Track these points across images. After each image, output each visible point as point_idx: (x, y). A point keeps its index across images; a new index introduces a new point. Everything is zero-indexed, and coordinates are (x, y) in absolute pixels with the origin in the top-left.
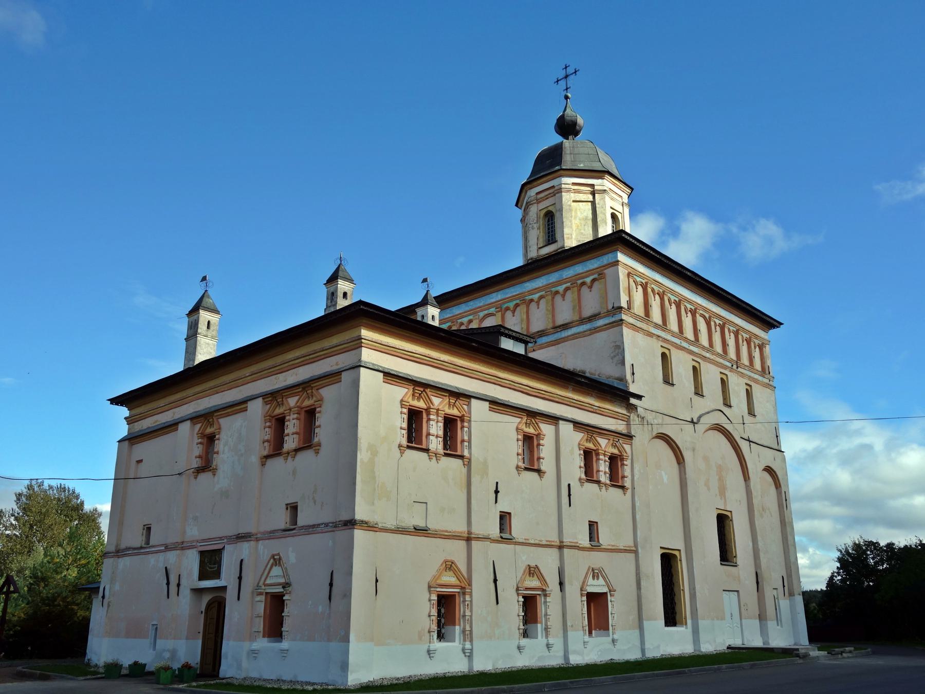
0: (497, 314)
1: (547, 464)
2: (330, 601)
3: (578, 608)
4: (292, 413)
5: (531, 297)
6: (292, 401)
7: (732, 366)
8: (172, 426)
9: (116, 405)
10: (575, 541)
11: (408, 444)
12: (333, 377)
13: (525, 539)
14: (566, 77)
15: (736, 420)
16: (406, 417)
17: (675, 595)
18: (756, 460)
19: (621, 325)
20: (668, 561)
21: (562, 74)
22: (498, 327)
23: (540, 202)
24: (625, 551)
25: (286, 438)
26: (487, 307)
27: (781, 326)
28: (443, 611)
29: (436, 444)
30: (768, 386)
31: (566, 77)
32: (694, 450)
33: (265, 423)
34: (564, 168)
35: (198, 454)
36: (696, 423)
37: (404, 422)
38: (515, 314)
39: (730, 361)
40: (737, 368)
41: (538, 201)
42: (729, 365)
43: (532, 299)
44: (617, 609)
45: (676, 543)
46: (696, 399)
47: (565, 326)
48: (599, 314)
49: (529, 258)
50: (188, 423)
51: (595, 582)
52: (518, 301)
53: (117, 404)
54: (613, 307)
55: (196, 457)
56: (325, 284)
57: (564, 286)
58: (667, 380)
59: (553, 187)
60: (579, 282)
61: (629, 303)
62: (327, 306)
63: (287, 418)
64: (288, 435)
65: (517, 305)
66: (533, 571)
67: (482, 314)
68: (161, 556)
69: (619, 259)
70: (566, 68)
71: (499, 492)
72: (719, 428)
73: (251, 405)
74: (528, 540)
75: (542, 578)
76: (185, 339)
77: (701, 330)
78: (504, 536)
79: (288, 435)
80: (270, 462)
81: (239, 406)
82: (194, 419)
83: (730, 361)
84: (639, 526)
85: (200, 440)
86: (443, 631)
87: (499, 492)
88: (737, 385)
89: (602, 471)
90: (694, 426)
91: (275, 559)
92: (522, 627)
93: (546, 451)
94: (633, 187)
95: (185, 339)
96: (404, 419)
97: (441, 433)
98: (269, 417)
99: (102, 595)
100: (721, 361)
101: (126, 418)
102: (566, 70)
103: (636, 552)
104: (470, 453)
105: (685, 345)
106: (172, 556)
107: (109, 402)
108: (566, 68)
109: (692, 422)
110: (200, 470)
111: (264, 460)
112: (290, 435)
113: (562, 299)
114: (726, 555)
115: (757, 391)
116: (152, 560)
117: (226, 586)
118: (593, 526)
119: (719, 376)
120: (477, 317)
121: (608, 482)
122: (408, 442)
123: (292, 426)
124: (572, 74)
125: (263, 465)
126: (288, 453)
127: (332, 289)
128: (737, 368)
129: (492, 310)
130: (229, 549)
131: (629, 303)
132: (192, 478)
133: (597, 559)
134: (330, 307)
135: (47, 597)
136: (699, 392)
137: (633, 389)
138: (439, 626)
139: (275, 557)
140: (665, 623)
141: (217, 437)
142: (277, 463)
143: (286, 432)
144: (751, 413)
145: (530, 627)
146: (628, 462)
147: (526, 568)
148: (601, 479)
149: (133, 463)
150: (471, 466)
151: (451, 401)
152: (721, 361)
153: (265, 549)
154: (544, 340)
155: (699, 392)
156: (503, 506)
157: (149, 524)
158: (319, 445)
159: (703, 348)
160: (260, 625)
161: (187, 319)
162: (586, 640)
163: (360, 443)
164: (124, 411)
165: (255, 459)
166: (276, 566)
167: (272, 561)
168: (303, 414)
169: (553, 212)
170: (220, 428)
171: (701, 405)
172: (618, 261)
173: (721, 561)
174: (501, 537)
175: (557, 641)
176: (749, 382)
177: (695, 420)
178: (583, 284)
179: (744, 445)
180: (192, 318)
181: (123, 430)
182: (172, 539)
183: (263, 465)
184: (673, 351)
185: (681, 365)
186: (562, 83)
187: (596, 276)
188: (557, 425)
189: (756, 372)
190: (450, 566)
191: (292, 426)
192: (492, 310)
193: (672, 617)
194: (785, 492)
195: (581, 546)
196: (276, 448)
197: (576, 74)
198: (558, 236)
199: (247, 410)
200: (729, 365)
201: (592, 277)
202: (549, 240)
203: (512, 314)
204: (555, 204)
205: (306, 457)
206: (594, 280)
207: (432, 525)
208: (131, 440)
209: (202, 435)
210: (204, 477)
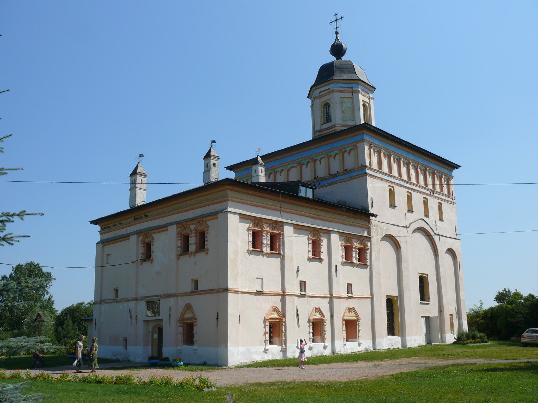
0: (297, 166)
1: (324, 256)
2: (217, 327)
3: (340, 329)
4: (192, 233)
5: (316, 158)
6: (192, 227)
7: (430, 193)
8: (126, 237)
9: (93, 224)
10: (340, 294)
11: (253, 249)
12: (215, 214)
13: (313, 294)
14: (336, 20)
15: (432, 225)
16: (251, 235)
17: (394, 320)
18: (442, 245)
19: (366, 175)
20: (390, 302)
21: (334, 19)
22: (298, 182)
23: (321, 97)
24: (367, 298)
25: (190, 246)
26: (291, 162)
27: (460, 167)
28: (272, 330)
29: (267, 249)
30: (450, 203)
31: (336, 20)
32: (406, 242)
33: (178, 238)
34: (335, 78)
35: (142, 253)
36: (408, 227)
37: (250, 238)
38: (308, 167)
39: (429, 190)
40: (433, 194)
41: (321, 97)
42: (428, 192)
43: (317, 159)
44: (364, 328)
45: (394, 293)
46: (409, 215)
47: (335, 176)
48: (354, 169)
49: (315, 130)
50: (136, 236)
51: (350, 314)
52: (309, 160)
53: (94, 224)
54: (362, 165)
55: (141, 254)
56: (203, 159)
57: (335, 152)
58: (392, 205)
59: (329, 89)
60: (343, 150)
61: (370, 163)
62: (204, 171)
63: (190, 236)
64: (191, 244)
65: (308, 162)
66: (318, 310)
67: (289, 167)
68: (126, 304)
69: (365, 138)
70: (336, 15)
71: (299, 271)
72: (421, 230)
73: (170, 228)
74: (314, 294)
75: (322, 314)
76: (129, 190)
77: (412, 174)
78: (303, 293)
79: (191, 244)
80: (181, 257)
81: (164, 228)
82: (138, 233)
83: (429, 190)
84: (374, 284)
85: (142, 245)
86: (272, 340)
87: (299, 271)
88: (433, 203)
89: (354, 257)
90: (407, 229)
91: (187, 306)
92: (311, 337)
93: (324, 248)
94: (375, 87)
95: (129, 190)
96: (250, 236)
97: (269, 242)
98: (179, 234)
99: (95, 323)
100: (424, 191)
101: (99, 232)
102: (336, 16)
103: (372, 299)
104: (284, 252)
105: (402, 183)
106: (132, 304)
107: (90, 223)
108: (336, 15)
109: (406, 227)
110: (143, 260)
111: (179, 257)
112: (192, 244)
113: (334, 159)
114: (424, 296)
115: (445, 205)
116: (121, 306)
117: (162, 319)
118: (349, 286)
119: (422, 200)
120: (286, 168)
121: (358, 262)
122: (252, 248)
123: (193, 240)
124: (340, 19)
125: (178, 259)
126: (191, 253)
127: (207, 162)
128: (433, 194)
129: (295, 165)
130: (163, 301)
131: (370, 163)
132: (139, 264)
133: (351, 303)
134: (206, 171)
135: (41, 326)
136: (410, 210)
137: (371, 211)
138: (270, 338)
139: (188, 305)
140: (388, 334)
141: (152, 244)
142: (185, 258)
143: (190, 243)
144: (441, 219)
145: (316, 337)
146: (368, 252)
147: (313, 308)
148: (354, 261)
149: (105, 256)
150: (284, 259)
151: (274, 225)
152: (424, 191)
153: (182, 302)
154: (325, 182)
155: (410, 210)
156: (301, 278)
157: (117, 288)
158: (208, 250)
159: (414, 184)
160: (181, 337)
161: (129, 178)
162: (345, 344)
163: (318, 353)
164: (98, 228)
165: (174, 256)
166: (188, 309)
167: (186, 307)
168: (198, 234)
169: (329, 104)
170: (153, 239)
171: (411, 217)
172: (364, 140)
173: (420, 301)
174: (300, 294)
175: (328, 343)
176: (440, 201)
177: (408, 226)
178: (345, 151)
179: (436, 238)
180: (132, 178)
181: (98, 238)
182: (132, 295)
183: (178, 259)
184: (396, 187)
185: (401, 194)
186: (334, 24)
187: (351, 147)
188: (329, 234)
189: (445, 195)
190: (275, 309)
191: (193, 240)
192: (295, 165)
193: (391, 331)
194: (459, 262)
195: (342, 296)
196: (185, 249)
197: (342, 20)
198: (332, 118)
199: (168, 230)
200: (428, 192)
201: (350, 148)
202: (327, 120)
203: (306, 167)
204: (330, 99)
205: (201, 256)
206: (351, 150)
207: (266, 290)
208: (103, 243)
209: (143, 242)
210: (147, 264)
